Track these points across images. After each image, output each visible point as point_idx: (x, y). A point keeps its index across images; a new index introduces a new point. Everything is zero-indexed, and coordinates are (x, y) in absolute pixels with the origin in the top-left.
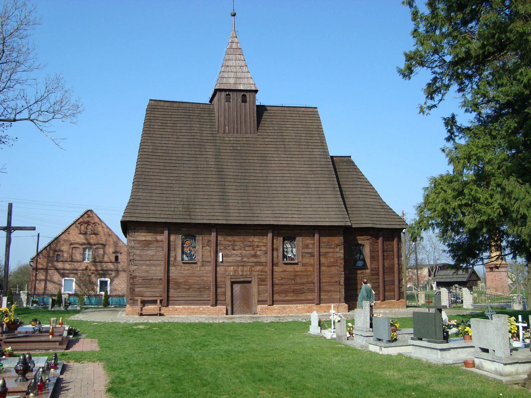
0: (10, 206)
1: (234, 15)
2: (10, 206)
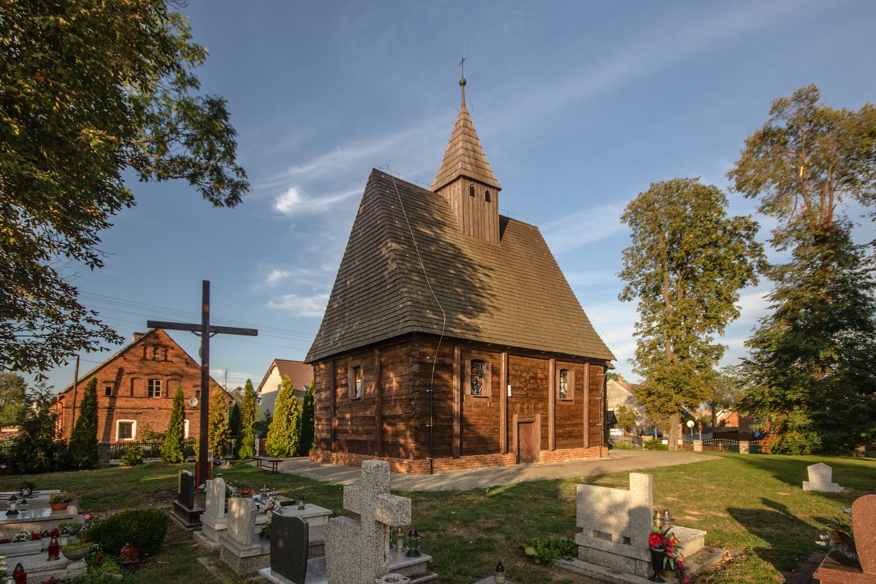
0: (254, 333)
1: (463, 84)
2: (254, 333)
